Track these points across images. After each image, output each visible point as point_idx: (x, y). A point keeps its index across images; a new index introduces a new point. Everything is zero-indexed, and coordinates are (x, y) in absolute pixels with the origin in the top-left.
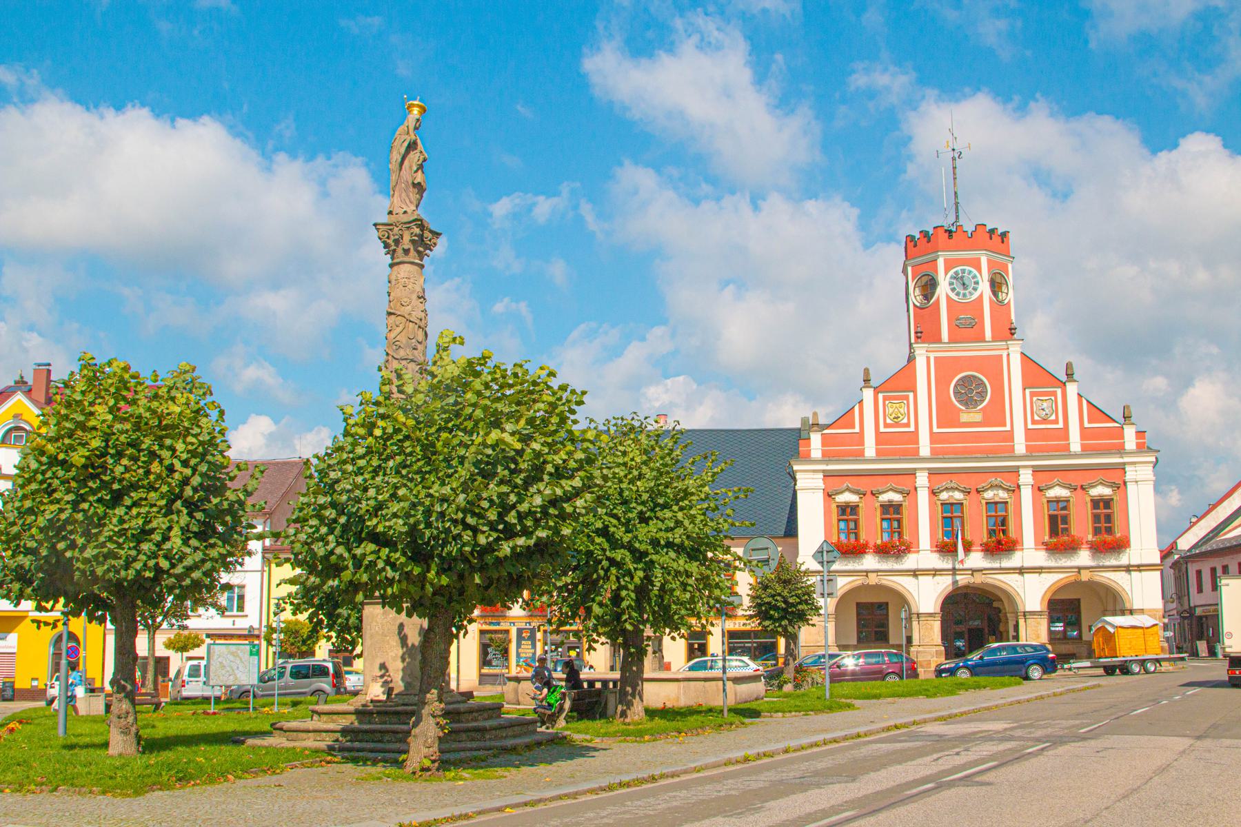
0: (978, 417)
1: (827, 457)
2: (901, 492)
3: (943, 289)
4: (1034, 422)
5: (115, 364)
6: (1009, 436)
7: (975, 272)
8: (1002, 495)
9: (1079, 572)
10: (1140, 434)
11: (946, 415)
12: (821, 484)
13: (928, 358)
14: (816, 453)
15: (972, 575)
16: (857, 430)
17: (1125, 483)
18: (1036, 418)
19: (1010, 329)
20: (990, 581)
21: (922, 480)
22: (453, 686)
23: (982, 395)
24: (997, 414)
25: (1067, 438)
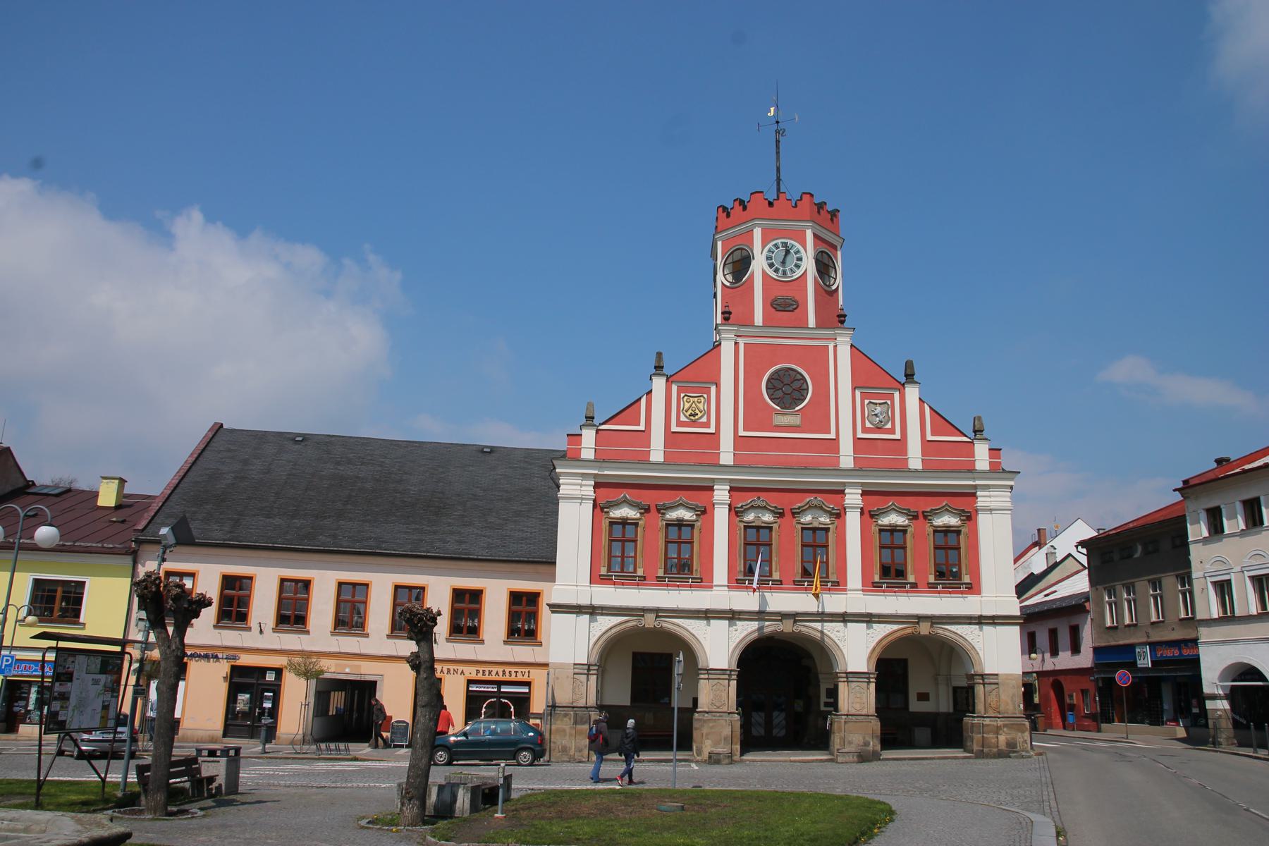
0: (795, 420)
1: (601, 459)
3: (759, 265)
6: (834, 444)
8: (825, 519)
10: (994, 452)
11: (754, 415)
12: (589, 491)
13: (736, 344)
14: (588, 454)
17: (845, 509)
21: (721, 494)
24: (820, 416)
25: (904, 450)
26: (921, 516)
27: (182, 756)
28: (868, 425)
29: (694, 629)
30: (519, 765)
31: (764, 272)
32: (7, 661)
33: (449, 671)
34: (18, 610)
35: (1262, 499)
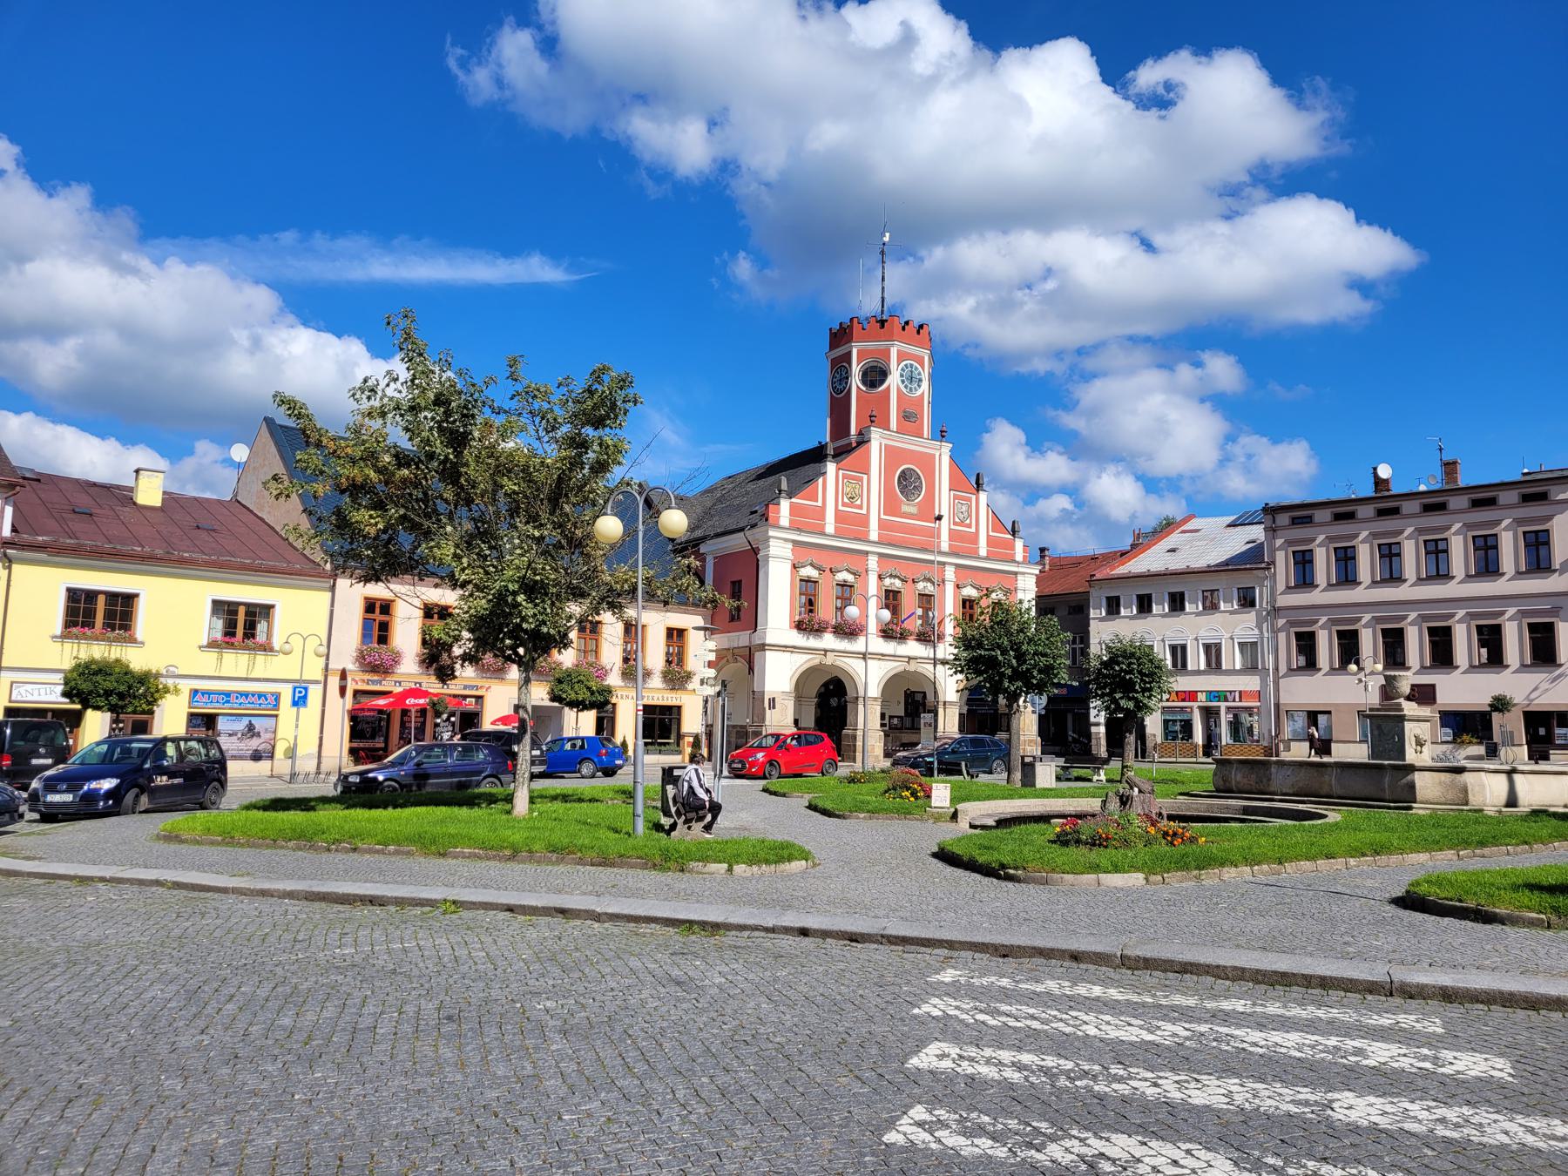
0: (913, 510)
1: (795, 527)
2: (854, 574)
3: (894, 381)
4: (955, 524)
5: (606, 378)
7: (920, 369)
9: (825, 655)
11: (890, 507)
12: (789, 554)
14: (785, 521)
15: (908, 662)
16: (820, 503)
17: (867, 571)
18: (957, 520)
19: (942, 432)
20: (838, 663)
22: (1551, 752)
23: (919, 488)
25: (823, 518)
26: (828, 570)
27: (1136, 743)
28: (957, 520)
29: (855, 667)
30: (583, 777)
31: (858, 387)
32: (300, 692)
33: (622, 696)
34: (305, 639)
35: (1153, 596)
